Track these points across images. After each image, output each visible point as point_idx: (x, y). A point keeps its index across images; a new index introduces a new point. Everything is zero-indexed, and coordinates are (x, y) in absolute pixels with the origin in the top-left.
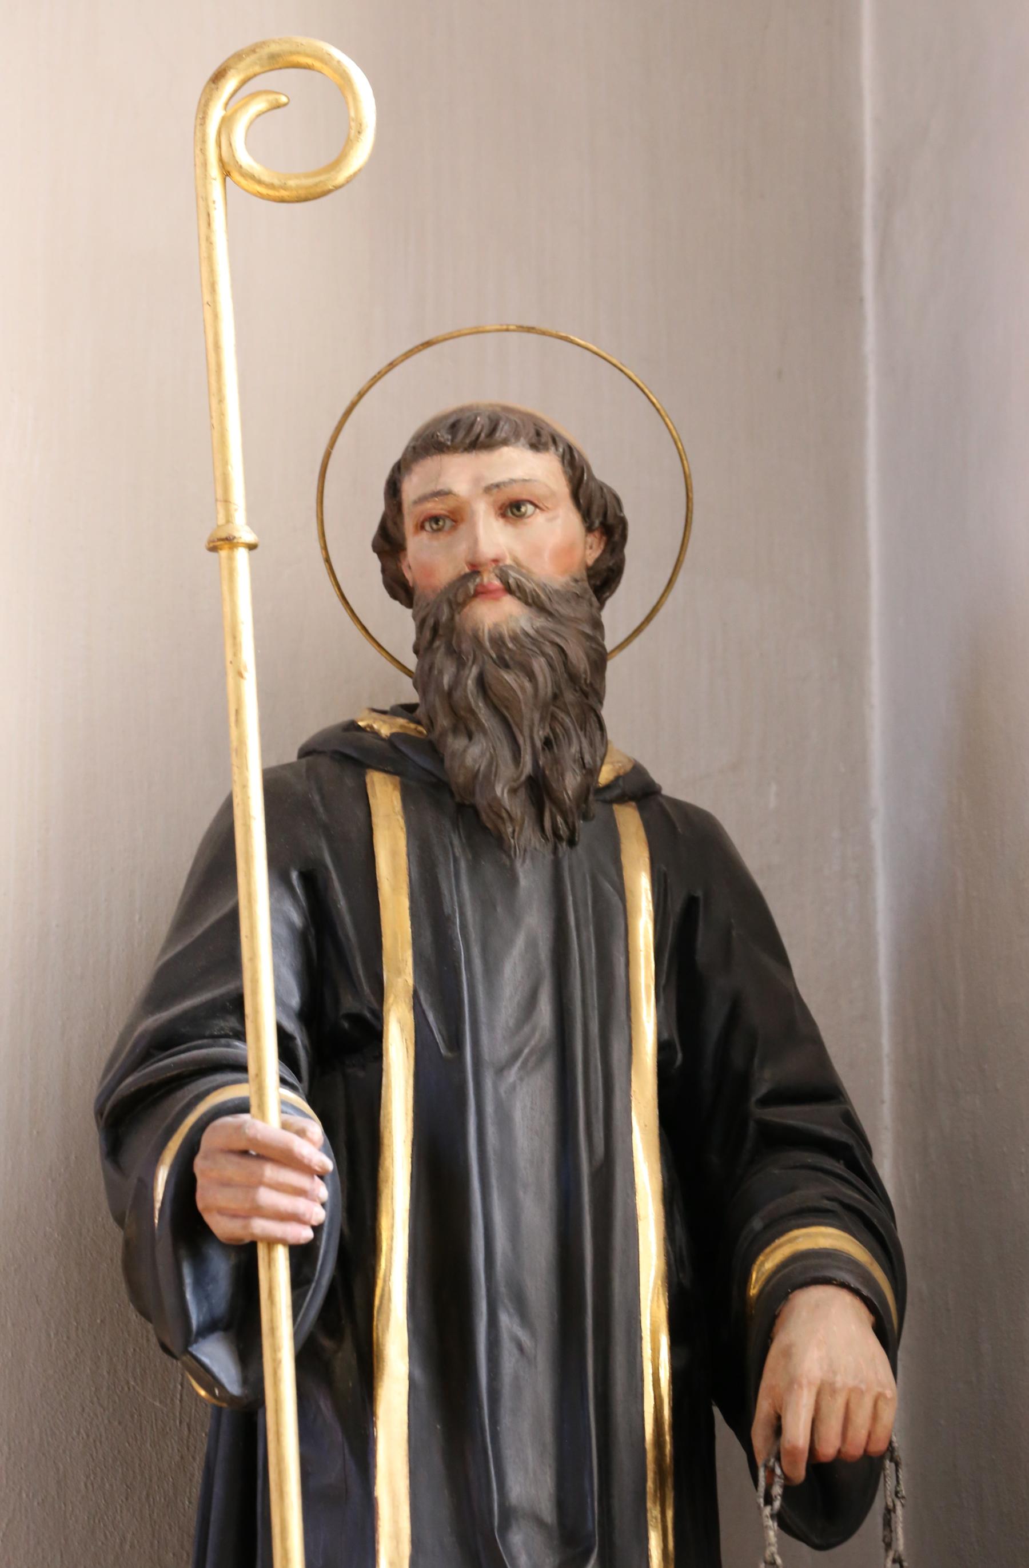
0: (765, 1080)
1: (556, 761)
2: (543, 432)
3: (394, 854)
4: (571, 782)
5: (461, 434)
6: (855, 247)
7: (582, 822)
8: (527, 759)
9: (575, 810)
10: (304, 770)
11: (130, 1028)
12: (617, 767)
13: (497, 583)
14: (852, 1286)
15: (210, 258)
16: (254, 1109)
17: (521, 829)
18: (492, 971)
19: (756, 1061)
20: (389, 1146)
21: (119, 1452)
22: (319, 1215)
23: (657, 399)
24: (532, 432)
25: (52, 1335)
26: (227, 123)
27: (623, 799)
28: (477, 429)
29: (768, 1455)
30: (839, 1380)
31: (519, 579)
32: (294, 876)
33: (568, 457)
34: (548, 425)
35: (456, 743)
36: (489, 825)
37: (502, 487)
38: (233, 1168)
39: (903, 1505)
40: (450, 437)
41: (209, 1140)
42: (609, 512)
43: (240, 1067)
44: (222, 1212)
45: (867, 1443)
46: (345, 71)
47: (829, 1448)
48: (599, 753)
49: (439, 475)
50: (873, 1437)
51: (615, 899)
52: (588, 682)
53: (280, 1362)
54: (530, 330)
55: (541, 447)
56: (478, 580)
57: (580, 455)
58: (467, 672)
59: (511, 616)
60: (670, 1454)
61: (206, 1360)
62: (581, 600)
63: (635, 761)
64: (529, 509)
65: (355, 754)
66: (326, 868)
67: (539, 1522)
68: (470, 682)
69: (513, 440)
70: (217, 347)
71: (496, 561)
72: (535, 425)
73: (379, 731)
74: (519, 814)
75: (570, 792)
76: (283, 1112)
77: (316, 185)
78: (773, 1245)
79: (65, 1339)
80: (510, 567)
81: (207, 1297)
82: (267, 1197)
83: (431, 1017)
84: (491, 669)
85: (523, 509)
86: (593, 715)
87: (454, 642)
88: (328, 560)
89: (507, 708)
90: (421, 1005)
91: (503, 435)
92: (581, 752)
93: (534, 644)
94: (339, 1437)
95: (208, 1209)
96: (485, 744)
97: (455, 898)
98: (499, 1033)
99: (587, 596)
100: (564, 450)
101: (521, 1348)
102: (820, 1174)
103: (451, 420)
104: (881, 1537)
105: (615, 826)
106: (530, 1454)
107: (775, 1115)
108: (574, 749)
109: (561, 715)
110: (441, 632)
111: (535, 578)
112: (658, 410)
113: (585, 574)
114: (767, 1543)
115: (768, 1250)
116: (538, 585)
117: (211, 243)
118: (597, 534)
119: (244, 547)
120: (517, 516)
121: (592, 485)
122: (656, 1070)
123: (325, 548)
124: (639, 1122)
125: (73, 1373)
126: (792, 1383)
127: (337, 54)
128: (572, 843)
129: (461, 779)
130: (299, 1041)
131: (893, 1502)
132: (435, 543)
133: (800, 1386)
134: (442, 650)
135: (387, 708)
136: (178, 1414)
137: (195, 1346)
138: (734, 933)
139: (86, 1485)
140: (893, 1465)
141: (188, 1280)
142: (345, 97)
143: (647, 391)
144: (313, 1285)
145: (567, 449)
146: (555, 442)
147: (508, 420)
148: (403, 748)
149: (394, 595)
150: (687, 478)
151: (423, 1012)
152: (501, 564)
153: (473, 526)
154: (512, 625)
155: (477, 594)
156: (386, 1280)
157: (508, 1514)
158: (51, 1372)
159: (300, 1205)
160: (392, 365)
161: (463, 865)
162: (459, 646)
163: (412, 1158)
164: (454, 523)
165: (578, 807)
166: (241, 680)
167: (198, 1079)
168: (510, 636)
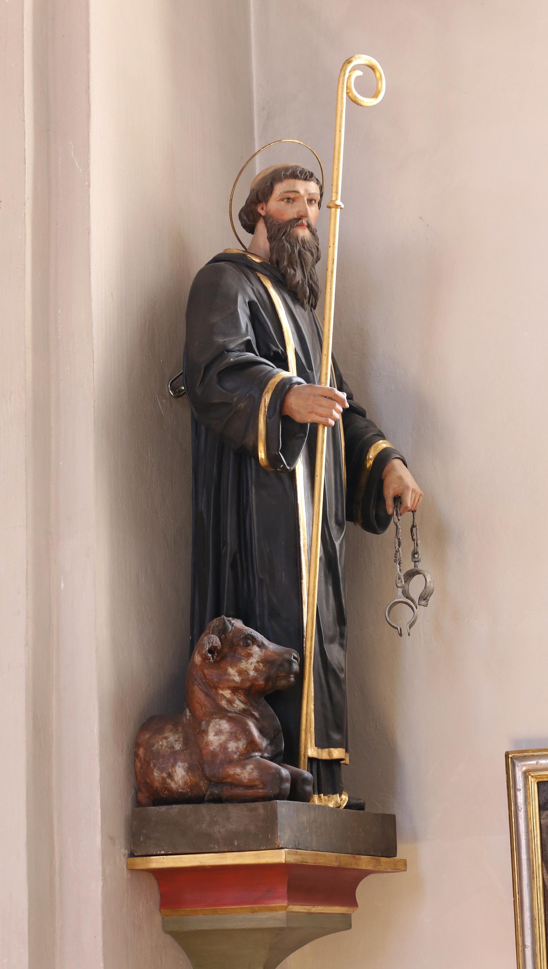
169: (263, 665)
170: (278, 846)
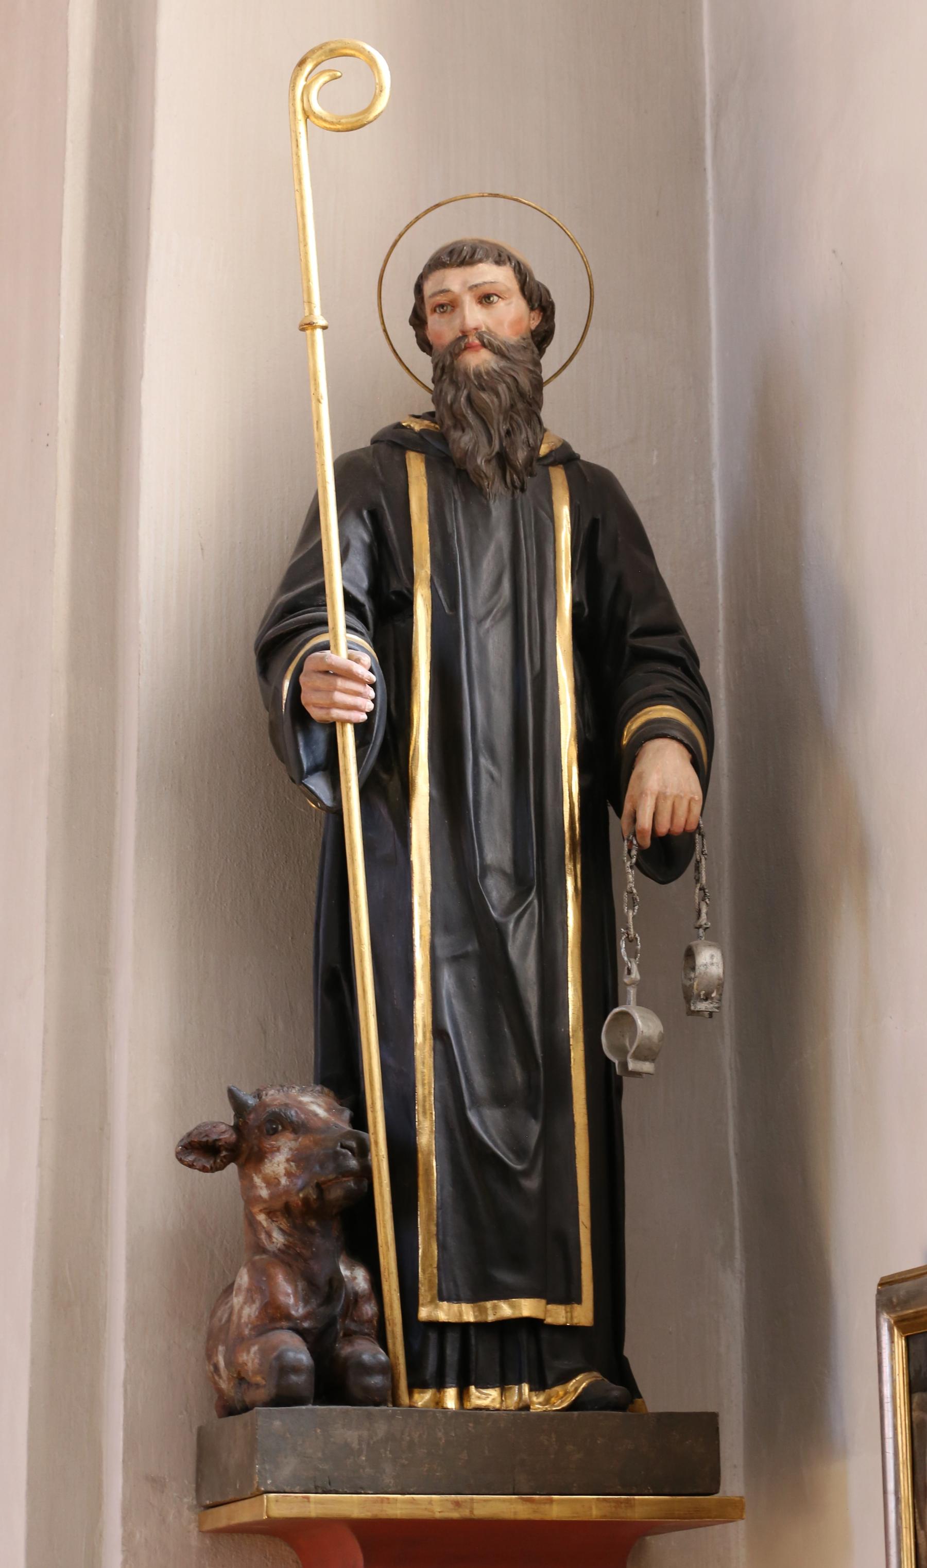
0: (635, 623)
1: (513, 443)
2: (502, 254)
3: (420, 499)
4: (521, 455)
5: (455, 257)
7: (529, 477)
9: (524, 471)
10: (371, 452)
11: (274, 601)
12: (551, 445)
13: (477, 342)
14: (678, 738)
15: (298, 165)
16: (332, 647)
17: (493, 483)
18: (476, 564)
19: (630, 612)
20: (417, 666)
21: (281, 837)
22: (370, 706)
23: (570, 233)
24: (496, 254)
25: (242, 773)
26: (307, 88)
27: (554, 464)
28: (464, 254)
29: (630, 833)
30: (669, 791)
31: (489, 339)
32: (365, 513)
33: (517, 268)
34: (506, 250)
35: (455, 434)
36: (475, 481)
37: (479, 286)
38: (320, 681)
39: (706, 859)
40: (449, 259)
41: (308, 665)
42: (543, 299)
43: (324, 622)
44: (315, 705)
46: (372, 57)
47: (663, 829)
48: (540, 437)
49: (443, 281)
50: (689, 822)
51: (548, 522)
52: (531, 397)
53: (350, 788)
55: (501, 263)
56: (466, 340)
57: (524, 265)
58: (461, 393)
59: (486, 361)
60: (579, 833)
62: (527, 350)
63: (564, 440)
64: (495, 298)
65: (399, 442)
66: (382, 507)
67: (504, 873)
68: (462, 399)
69: (485, 259)
70: (303, 215)
71: (476, 329)
72: (498, 250)
73: (414, 428)
74: (491, 474)
75: (520, 461)
76: (349, 648)
77: (357, 121)
78: (636, 716)
79: (249, 774)
80: (485, 332)
81: (313, 752)
82: (339, 697)
83: (440, 592)
84: (474, 391)
85: (491, 299)
86: (535, 416)
87: (454, 377)
88: (385, 331)
89: (484, 413)
90: (435, 585)
91: (479, 257)
92: (527, 437)
93: (499, 377)
94: (391, 828)
95: (308, 704)
96: (471, 435)
97: (455, 524)
98: (480, 601)
99: (531, 348)
100: (515, 264)
101: (492, 777)
102: (665, 676)
103: (449, 249)
104: (693, 877)
105: (550, 478)
106: (498, 836)
107: (641, 642)
108: (524, 436)
109: (516, 416)
110: (446, 370)
111: (499, 338)
112: (571, 239)
113: (529, 335)
114: (628, 882)
116: (501, 342)
117: (299, 157)
118: (537, 311)
119: (320, 328)
120: (488, 303)
121: (532, 283)
122: (571, 619)
123: (383, 323)
125: (254, 793)
126: (642, 793)
127: (368, 48)
128: (523, 490)
129: (458, 455)
130: (367, 607)
131: (700, 857)
132: (442, 320)
133: (646, 795)
134: (448, 381)
135: (420, 414)
136: (314, 815)
137: (306, 780)
138: (620, 539)
139: (263, 855)
140: (700, 837)
141: (301, 744)
142: (373, 71)
143: (565, 229)
144: (371, 745)
145: (517, 264)
146: (509, 260)
147: (482, 248)
148: (427, 438)
149: (423, 350)
150: (590, 277)
151: (436, 589)
153: (463, 310)
154: (486, 365)
155: (466, 348)
156: (416, 742)
157: (485, 869)
158: (242, 793)
159: (359, 701)
160: (418, 218)
161: (459, 504)
162: (457, 378)
163: (430, 672)
164: (453, 308)
165: (526, 469)
166: (320, 404)
167: (308, 630)
168: (485, 372)
169: (295, 1165)
170: (258, 1489)
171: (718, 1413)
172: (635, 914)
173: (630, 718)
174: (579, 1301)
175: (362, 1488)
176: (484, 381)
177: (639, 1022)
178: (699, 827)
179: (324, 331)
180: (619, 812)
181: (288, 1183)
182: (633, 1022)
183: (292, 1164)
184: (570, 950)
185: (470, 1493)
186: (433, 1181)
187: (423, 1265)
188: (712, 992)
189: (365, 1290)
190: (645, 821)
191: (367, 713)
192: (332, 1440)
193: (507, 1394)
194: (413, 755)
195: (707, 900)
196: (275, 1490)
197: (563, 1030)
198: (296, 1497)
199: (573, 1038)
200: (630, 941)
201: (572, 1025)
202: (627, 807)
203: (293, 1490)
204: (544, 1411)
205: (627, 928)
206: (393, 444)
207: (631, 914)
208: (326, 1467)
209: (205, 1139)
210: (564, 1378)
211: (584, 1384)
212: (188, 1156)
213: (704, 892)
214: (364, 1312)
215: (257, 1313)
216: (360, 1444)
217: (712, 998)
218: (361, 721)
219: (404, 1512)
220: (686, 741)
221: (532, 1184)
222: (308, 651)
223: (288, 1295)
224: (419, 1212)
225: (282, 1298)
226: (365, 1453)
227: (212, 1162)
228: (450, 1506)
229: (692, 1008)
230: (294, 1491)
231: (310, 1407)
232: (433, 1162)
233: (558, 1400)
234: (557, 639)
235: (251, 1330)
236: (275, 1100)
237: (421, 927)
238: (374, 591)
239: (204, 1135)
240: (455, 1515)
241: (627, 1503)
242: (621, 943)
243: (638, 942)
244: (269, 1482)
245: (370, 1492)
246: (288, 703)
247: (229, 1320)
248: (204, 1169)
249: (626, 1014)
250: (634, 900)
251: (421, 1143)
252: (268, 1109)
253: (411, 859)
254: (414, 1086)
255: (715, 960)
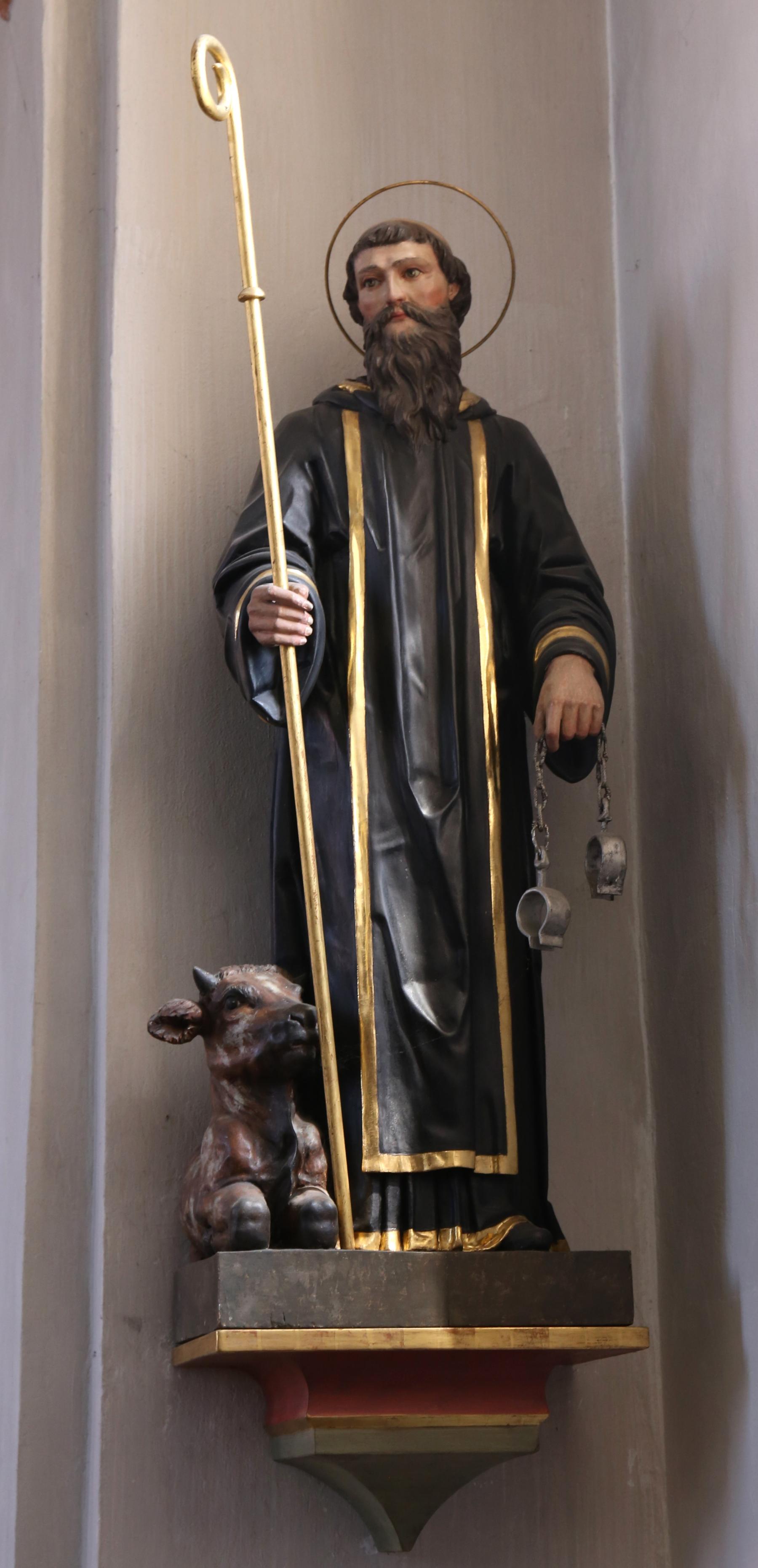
6: (605, 130)
8: (420, 400)
27: (473, 418)
28: (388, 233)
32: (307, 465)
35: (384, 394)
41: (253, 594)
43: (267, 560)
45: (590, 730)
47: (570, 732)
54: (435, 183)
56: (392, 311)
61: (262, 704)
64: (417, 272)
65: (336, 402)
66: (321, 459)
76: (290, 581)
80: (408, 303)
82: (281, 623)
83: (372, 532)
85: (413, 273)
103: (376, 230)
104: (595, 777)
107: (549, 572)
109: (437, 377)
113: (448, 304)
115: (543, 639)
124: (479, 578)
128: (444, 441)
137: (256, 697)
141: (251, 666)
144: (312, 665)
148: (361, 398)
152: (403, 302)
159: (299, 626)
171: (630, 1251)
172: (544, 807)
173: (540, 639)
174: (505, 1153)
175: (313, 1323)
176: (407, 344)
177: (549, 902)
178: (601, 732)
179: (262, 301)
180: (532, 718)
181: (246, 1052)
182: (543, 902)
183: (250, 1034)
184: (491, 842)
185: (305, 1325)
186: (373, 1047)
187: (366, 1122)
188: (616, 878)
189: (315, 1145)
190: (553, 726)
191: (307, 637)
192: (286, 1279)
193: (442, 1236)
194: (351, 674)
195: (608, 797)
196: (236, 1326)
197: (486, 912)
198: (245, 1332)
199: (495, 919)
200: (541, 830)
201: (494, 908)
202: (538, 715)
203: (252, 1326)
204: (475, 1251)
205: (538, 820)
206: (332, 405)
207: (540, 807)
208: (281, 1304)
209: (173, 1015)
210: (493, 1223)
211: (511, 1227)
212: (159, 1029)
213: (606, 790)
214: (315, 1165)
215: (220, 1168)
216: (311, 1283)
217: (616, 883)
218: (301, 644)
219: (341, 1344)
220: (589, 657)
221: (460, 1048)
222: (257, 583)
223: (248, 1151)
224: (361, 1075)
225: (242, 1154)
226: (315, 1291)
227: (180, 1035)
228: (384, 1338)
229: (599, 891)
230: (253, 1327)
231: (267, 1250)
232: (373, 1031)
233: (488, 1241)
234: (476, 570)
235: (215, 1183)
236: (235, 978)
237: (360, 825)
238: (314, 533)
239: (172, 1010)
240: (387, 1346)
241: (542, 1334)
242: (532, 833)
243: (547, 831)
244: (230, 1319)
245: (321, 1327)
246: (239, 633)
247: (198, 1175)
248: (173, 1042)
249: (536, 895)
250: (543, 795)
251: (362, 1014)
252: (229, 987)
253: (350, 765)
254: (356, 964)
255: (619, 849)
